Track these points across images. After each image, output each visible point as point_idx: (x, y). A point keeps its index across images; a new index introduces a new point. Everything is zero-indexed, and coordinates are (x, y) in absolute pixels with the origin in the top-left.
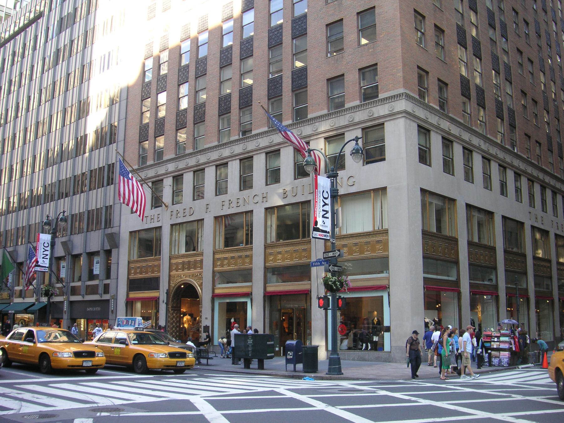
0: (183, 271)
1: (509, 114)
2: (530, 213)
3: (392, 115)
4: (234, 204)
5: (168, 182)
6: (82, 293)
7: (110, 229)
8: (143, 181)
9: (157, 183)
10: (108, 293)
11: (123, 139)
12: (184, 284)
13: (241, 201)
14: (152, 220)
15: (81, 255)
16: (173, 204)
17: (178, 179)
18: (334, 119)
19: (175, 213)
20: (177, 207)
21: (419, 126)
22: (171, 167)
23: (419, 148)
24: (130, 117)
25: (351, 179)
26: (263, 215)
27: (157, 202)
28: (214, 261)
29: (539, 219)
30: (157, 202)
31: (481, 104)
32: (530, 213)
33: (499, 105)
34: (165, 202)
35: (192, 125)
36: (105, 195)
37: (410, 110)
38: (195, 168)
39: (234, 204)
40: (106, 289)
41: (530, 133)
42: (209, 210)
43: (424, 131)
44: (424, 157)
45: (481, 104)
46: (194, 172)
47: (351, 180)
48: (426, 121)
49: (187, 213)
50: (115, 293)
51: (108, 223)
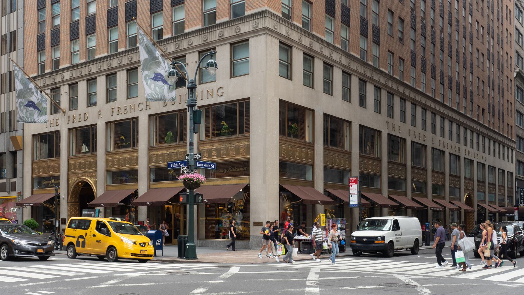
0: (80, 170)
1: (373, 32)
2: (387, 122)
3: (256, 32)
4: (77, 120)
5: (65, 90)
6: (7, 189)
7: (14, 132)
8: (41, 89)
9: (55, 90)
10: (15, 190)
11: (22, 47)
12: (80, 182)
13: (128, 108)
14: (52, 125)
15: (5, 153)
16: (70, 110)
17: (73, 86)
18: (206, 34)
19: (71, 118)
20: (73, 113)
21: (280, 42)
22: (67, 75)
23: (280, 63)
24: (27, 26)
25: (221, 90)
26: (146, 121)
27: (56, 108)
28: (107, 162)
29: (397, 128)
30: (56, 108)
31: (346, 21)
32: (387, 122)
33: (364, 23)
34: (62, 109)
35: (84, 36)
36: (9, 99)
37: (271, 27)
38: (88, 77)
39: (77, 120)
40: (13, 187)
41: (393, 50)
42: (101, 116)
43: (286, 47)
44: (286, 70)
45: (346, 21)
46: (88, 81)
47: (221, 91)
48: (288, 38)
49: (82, 118)
50: (21, 190)
51: (12, 128)
